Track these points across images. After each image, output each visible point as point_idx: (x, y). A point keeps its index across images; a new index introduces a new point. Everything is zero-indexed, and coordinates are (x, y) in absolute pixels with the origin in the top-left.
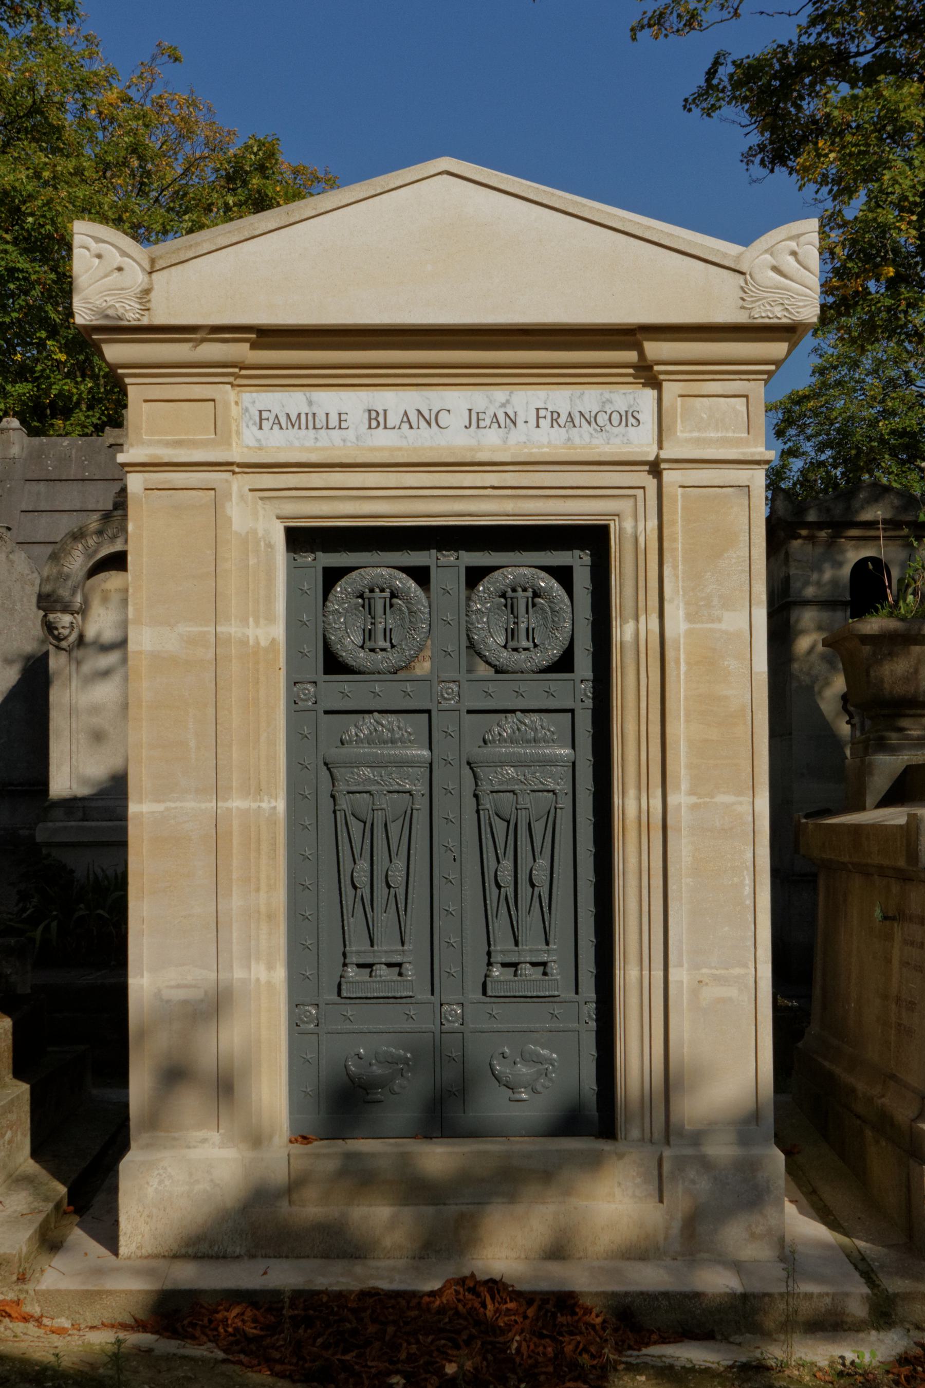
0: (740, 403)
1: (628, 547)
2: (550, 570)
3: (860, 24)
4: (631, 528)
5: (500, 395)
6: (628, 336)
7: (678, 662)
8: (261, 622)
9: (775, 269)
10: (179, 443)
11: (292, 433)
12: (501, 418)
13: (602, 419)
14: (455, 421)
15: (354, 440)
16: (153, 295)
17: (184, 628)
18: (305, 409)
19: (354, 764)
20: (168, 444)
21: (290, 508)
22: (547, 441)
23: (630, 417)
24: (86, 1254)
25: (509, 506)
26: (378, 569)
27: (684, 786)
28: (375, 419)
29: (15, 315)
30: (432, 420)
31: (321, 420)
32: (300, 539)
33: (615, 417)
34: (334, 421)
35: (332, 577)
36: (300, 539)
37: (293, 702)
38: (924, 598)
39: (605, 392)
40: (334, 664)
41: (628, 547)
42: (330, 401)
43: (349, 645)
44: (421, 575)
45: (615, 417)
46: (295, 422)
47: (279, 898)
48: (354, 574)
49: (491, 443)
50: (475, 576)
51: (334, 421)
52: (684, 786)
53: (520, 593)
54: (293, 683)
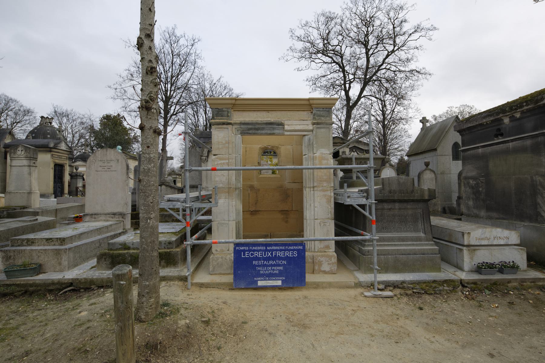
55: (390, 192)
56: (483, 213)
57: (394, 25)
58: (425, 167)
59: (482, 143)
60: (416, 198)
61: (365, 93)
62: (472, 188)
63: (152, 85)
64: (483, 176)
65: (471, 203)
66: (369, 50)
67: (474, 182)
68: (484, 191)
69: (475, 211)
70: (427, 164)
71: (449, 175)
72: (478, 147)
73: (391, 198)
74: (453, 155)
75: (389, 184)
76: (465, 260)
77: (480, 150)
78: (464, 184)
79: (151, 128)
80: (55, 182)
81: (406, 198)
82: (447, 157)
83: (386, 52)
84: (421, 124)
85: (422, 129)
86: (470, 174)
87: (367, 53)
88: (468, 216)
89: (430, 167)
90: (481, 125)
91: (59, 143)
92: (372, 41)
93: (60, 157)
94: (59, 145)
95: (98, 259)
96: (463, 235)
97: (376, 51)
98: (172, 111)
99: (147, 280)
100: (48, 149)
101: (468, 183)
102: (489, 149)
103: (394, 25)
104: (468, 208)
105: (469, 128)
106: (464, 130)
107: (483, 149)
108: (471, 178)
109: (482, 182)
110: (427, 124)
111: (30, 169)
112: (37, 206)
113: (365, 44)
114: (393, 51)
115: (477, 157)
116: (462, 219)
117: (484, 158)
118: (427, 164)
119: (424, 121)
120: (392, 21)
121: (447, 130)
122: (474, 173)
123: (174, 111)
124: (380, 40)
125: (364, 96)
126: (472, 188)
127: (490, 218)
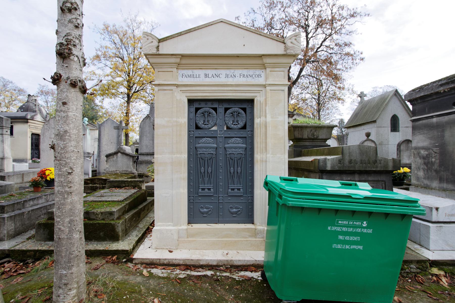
0: (282, 73)
1: (259, 103)
2: (241, 108)
3: (177, 272)
4: (259, 99)
5: (232, 71)
6: (261, 56)
7: (269, 127)
8: (182, 118)
9: (291, 43)
10: (165, 80)
11: (189, 78)
12: (233, 76)
13: (254, 76)
14: (223, 76)
15: (202, 80)
16: (159, 47)
17: (166, 119)
18: (191, 74)
19: (201, 148)
20: (163, 81)
21: (189, 94)
22: (242, 81)
23: (259, 76)
24: (437, 209)
25: (234, 94)
26: (206, 108)
27: (270, 153)
28: (206, 76)
29: (198, 293)
30: (218, 76)
31: (195, 76)
32: (191, 102)
33: (256, 76)
34: (198, 76)
35: (197, 109)
36: (191, 102)
37: (189, 135)
38: (137, 302)
39: (254, 70)
40: (197, 127)
41: (259, 103)
42: (197, 72)
43: (201, 124)
44: (215, 109)
45: (256, 76)
46: (190, 76)
47: (186, 175)
48: (202, 109)
49: (230, 81)
50: (226, 109)
51: (198, 76)
52: (270, 153)
53: (235, 113)
54: (189, 131)
55: (350, 162)
56: (435, 184)
57: (332, 11)
58: (366, 138)
59: (433, 112)
60: (378, 169)
61: (303, 73)
62: (424, 158)
63: (71, 26)
64: (436, 147)
65: (421, 174)
66: (309, 34)
67: (426, 153)
68: (438, 161)
69: (426, 182)
70: (368, 135)
71: (387, 146)
72: (432, 117)
73: (351, 169)
74: (391, 127)
75: (350, 153)
76: (431, 237)
77: (435, 120)
78: (414, 154)
79: (68, 78)
80: (32, 149)
81: (368, 169)
82: (386, 128)
83: (324, 36)
84: (359, 99)
85: (360, 103)
86: (421, 144)
87: (307, 36)
88: (417, 186)
89: (370, 138)
90: (437, 93)
91: (34, 115)
92: (312, 24)
93: (36, 128)
94: (35, 117)
95: (36, 230)
96: (431, 211)
97: (315, 35)
98: (134, 90)
99: (64, 268)
100: (26, 120)
101: (419, 153)
102: (446, 118)
103: (332, 11)
104: (418, 179)
105: (421, 98)
106: (416, 99)
107: (438, 118)
108: (423, 148)
109: (436, 153)
110: (364, 98)
111: (3, 137)
112: (11, 170)
113: (306, 28)
114: (330, 35)
115: (431, 127)
116: (410, 189)
117: (440, 127)
118: (368, 135)
119: (361, 95)
120: (331, 7)
121: (386, 102)
122: (426, 143)
123: (136, 89)
124: (320, 24)
125: (303, 76)
126: (424, 158)
127: (444, 190)
